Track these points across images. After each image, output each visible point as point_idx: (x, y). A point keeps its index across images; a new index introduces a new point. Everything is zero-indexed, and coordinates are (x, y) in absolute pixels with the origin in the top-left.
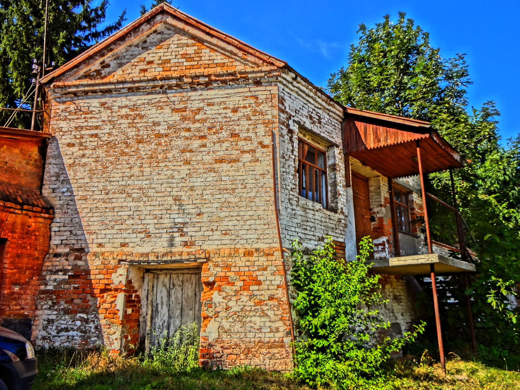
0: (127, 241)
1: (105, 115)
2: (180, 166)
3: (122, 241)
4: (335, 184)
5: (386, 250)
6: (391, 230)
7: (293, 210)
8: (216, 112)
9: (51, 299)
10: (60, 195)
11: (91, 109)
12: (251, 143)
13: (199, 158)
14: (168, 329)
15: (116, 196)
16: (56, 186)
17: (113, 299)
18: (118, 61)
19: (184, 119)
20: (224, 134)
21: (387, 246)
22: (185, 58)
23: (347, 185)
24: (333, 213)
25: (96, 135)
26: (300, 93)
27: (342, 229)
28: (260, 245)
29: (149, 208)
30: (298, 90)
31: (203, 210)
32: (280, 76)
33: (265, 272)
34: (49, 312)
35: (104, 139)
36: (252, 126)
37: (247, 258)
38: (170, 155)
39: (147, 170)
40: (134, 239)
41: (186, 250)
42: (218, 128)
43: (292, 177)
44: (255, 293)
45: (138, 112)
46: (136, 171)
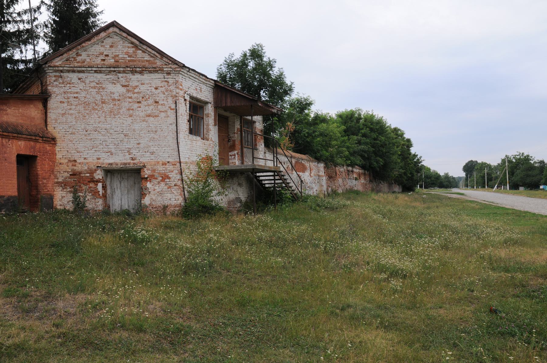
0: (100, 157)
1: (81, 86)
3: (98, 157)
6: (240, 147)
9: (61, 186)
11: (73, 81)
13: (137, 114)
20: (151, 101)
21: (236, 156)
23: (215, 125)
25: (77, 97)
26: (191, 77)
28: (169, 160)
34: (61, 192)
39: (108, 119)
42: (147, 97)
46: (102, 119)
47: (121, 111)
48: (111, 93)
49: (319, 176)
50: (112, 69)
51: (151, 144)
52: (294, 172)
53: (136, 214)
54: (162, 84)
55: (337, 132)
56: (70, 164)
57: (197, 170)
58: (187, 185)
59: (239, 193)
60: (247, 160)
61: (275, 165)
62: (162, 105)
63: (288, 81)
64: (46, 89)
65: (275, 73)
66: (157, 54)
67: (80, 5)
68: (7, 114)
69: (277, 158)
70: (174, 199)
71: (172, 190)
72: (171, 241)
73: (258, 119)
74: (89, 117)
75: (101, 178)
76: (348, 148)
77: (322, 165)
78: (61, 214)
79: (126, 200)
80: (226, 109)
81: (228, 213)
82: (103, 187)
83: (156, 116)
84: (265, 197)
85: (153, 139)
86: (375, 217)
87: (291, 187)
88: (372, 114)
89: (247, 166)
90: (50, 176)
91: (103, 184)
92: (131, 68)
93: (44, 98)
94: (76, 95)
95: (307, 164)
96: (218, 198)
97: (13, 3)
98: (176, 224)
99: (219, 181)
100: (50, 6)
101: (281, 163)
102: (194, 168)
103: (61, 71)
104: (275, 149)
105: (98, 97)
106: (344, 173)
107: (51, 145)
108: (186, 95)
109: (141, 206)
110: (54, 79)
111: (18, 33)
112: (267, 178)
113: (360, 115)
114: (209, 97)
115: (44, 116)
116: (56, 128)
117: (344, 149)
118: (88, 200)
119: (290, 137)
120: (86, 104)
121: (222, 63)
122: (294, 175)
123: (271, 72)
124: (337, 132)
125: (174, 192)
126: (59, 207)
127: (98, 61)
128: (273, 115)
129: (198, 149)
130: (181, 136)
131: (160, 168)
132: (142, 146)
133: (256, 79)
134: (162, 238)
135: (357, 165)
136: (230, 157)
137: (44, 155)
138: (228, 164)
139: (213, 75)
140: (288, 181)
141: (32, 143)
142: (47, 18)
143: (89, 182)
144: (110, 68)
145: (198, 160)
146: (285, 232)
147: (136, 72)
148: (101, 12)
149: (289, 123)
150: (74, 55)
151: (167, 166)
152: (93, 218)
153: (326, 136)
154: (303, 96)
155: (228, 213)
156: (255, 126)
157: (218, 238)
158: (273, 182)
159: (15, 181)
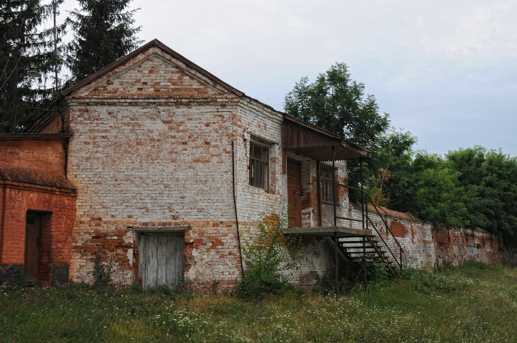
0: (132, 214)
2: (169, 163)
4: (274, 173)
5: (311, 218)
6: (316, 202)
7: (245, 195)
8: (194, 125)
9: (81, 252)
10: (81, 180)
11: (101, 116)
12: (218, 150)
13: (182, 158)
14: (157, 273)
15: (123, 182)
16: (77, 173)
17: (125, 253)
18: (120, 81)
19: (171, 128)
20: (199, 142)
22: (171, 82)
23: (284, 173)
24: (272, 195)
26: (252, 110)
27: (278, 205)
29: (147, 192)
30: (250, 109)
31: (186, 195)
32: (239, 102)
33: (227, 237)
34: (80, 260)
35: (112, 140)
36: (219, 138)
37: (215, 228)
38: (161, 155)
40: (136, 212)
41: (173, 221)
42: (195, 137)
43: (245, 173)
44: (219, 250)
45: (136, 122)
46: (137, 165)
94: (104, 134)
105: (133, 137)
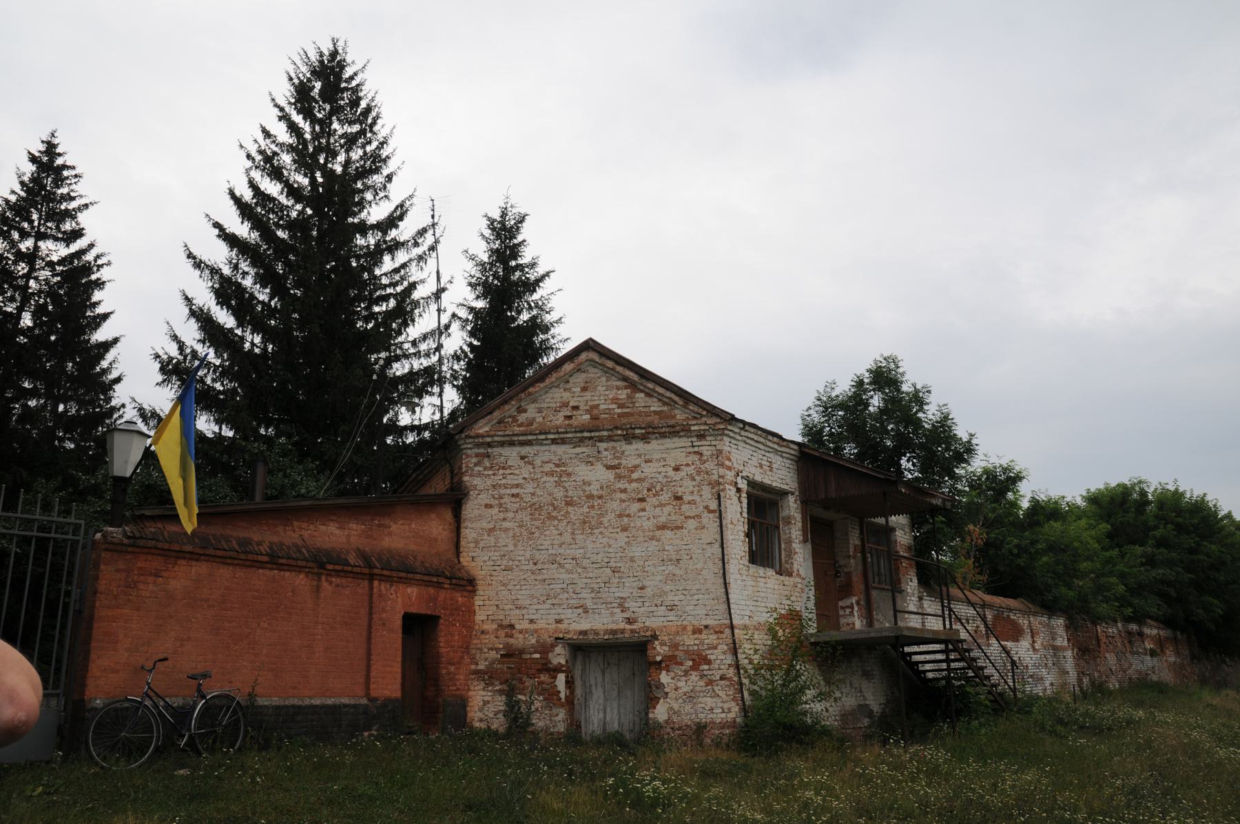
0: (563, 617)
1: (526, 471)
3: (557, 617)
6: (862, 587)
11: (510, 463)
23: (805, 541)
28: (709, 622)
42: (658, 488)
46: (567, 537)
47: (605, 520)
48: (584, 483)
49: (1055, 648)
50: (586, 434)
51: (668, 588)
52: (993, 641)
53: (638, 741)
54: (689, 460)
55: (1089, 539)
56: (502, 633)
57: (769, 642)
58: (749, 676)
59: (865, 694)
60: (880, 617)
61: (948, 626)
62: (689, 503)
63: (961, 432)
64: (461, 482)
65: (931, 417)
66: (677, 399)
67: (519, 312)
68: (390, 534)
69: (950, 610)
70: (722, 709)
71: (716, 688)
72: (718, 804)
73: (899, 521)
74: (541, 534)
75: (563, 662)
76: (1122, 576)
77: (1059, 622)
78: (482, 739)
79: (616, 711)
80: (827, 504)
81: (842, 741)
82: (567, 682)
83: (678, 528)
84: (929, 703)
85: (672, 578)
86: (1222, 753)
87: (988, 678)
88: (1177, 490)
89: (881, 630)
90: (462, 657)
91: (567, 677)
92: (622, 430)
93: (456, 499)
94: (515, 491)
95: (1023, 622)
96: (818, 707)
97: (407, 325)
98: (726, 767)
99: (820, 666)
100: (467, 320)
101: (960, 620)
102: (762, 639)
103: (489, 445)
104: (944, 589)
105: (559, 493)
106: (1118, 639)
107: (466, 594)
108: (739, 480)
109: (647, 724)
110: (474, 460)
111: (412, 376)
112: (928, 657)
113: (1143, 494)
114: (788, 481)
115: (454, 535)
116: (478, 558)
117: (1113, 580)
118: (537, 710)
119: (977, 559)
120: (535, 508)
121: (811, 405)
122: (994, 648)
123: (920, 415)
124: (1089, 539)
125: (720, 693)
126: (477, 725)
127: (559, 419)
128: (934, 510)
129: (766, 598)
130: (732, 568)
131: (689, 641)
132: (648, 592)
133: (887, 432)
134: (696, 797)
135: (1151, 618)
136: (841, 613)
137: (452, 614)
138: (837, 627)
139: (794, 433)
140: (981, 663)
141: (432, 590)
142: (461, 343)
143: (540, 671)
144: (582, 432)
145: (771, 620)
146: (982, 787)
147: (634, 437)
148: (559, 321)
149: (971, 527)
150: (513, 412)
151: (703, 636)
152: (547, 750)
153: (1064, 551)
154: (997, 462)
155: (842, 741)
156: (893, 538)
157: (824, 800)
158: (944, 666)
159: (397, 668)
